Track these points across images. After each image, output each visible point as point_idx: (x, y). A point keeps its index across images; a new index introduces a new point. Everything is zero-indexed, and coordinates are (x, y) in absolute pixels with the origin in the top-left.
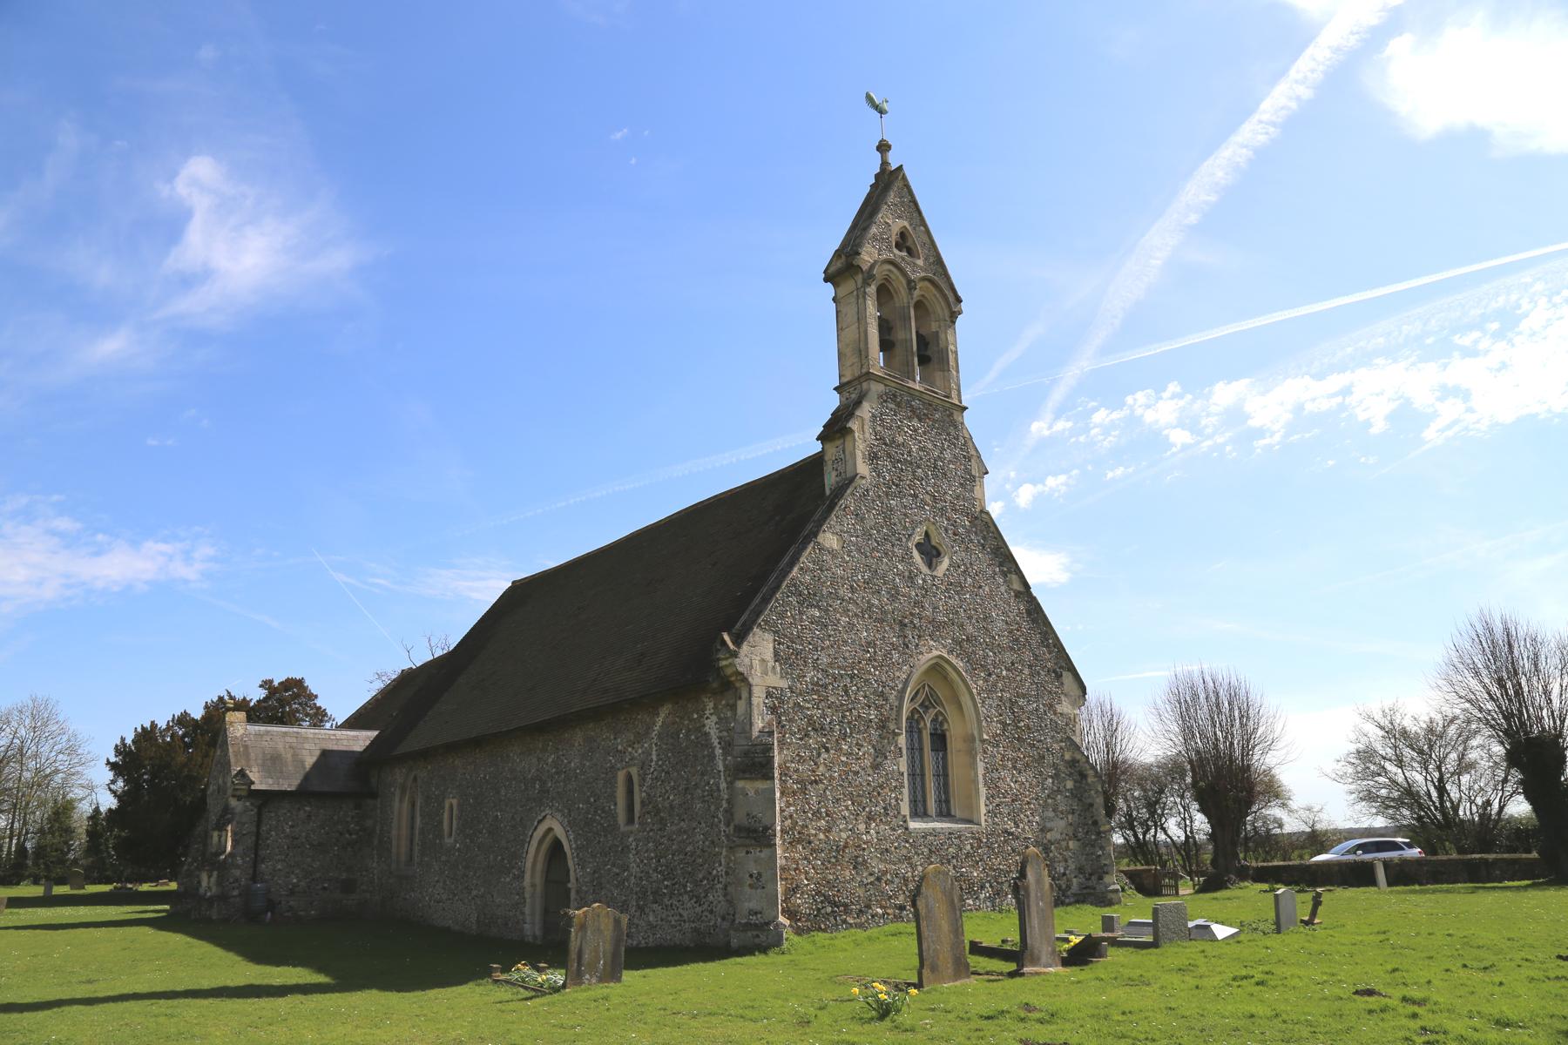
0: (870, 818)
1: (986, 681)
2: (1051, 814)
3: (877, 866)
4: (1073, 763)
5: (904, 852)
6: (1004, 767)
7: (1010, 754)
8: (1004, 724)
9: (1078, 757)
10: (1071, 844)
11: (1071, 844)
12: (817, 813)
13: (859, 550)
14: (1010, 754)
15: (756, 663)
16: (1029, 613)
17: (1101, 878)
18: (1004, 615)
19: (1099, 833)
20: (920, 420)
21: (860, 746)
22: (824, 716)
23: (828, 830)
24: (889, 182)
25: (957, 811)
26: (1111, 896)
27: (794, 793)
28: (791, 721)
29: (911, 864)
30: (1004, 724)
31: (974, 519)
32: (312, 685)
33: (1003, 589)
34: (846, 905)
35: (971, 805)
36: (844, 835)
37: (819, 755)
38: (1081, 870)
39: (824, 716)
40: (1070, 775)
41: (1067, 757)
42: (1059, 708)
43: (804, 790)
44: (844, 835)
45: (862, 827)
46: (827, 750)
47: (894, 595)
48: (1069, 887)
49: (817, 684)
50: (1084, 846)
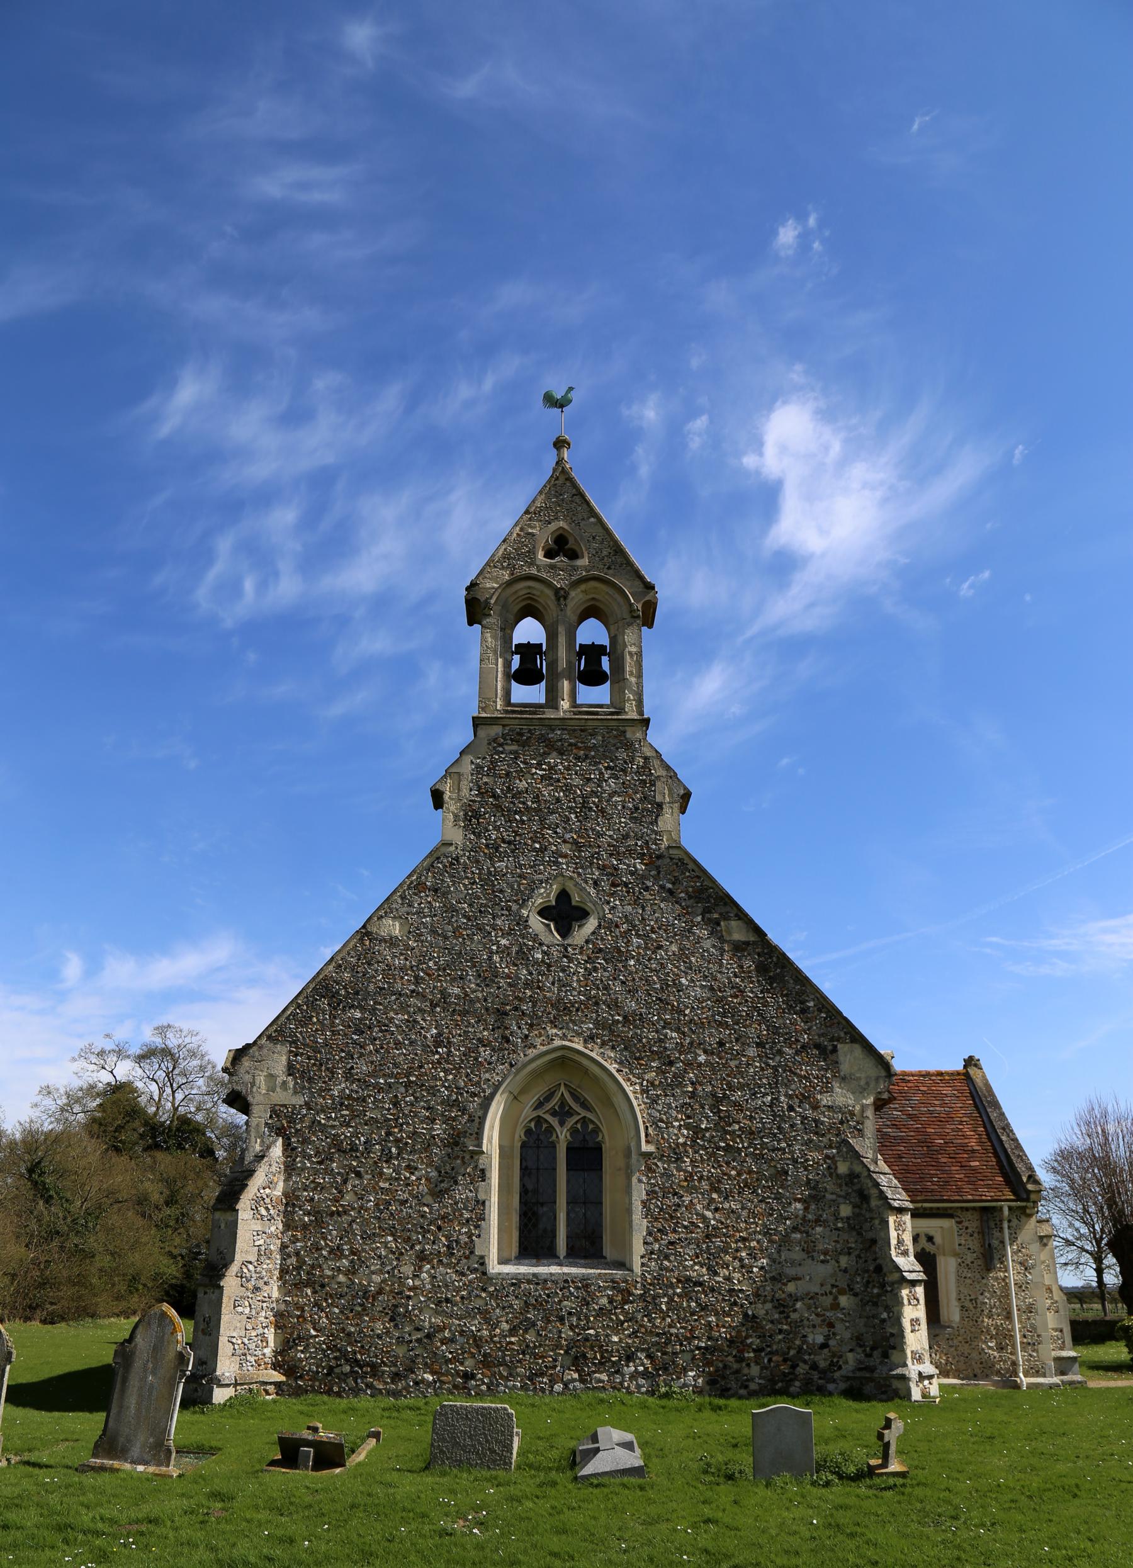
0: (422, 1257)
1: (660, 1072)
2: (797, 1254)
3: (428, 1320)
4: (852, 1177)
5: (478, 1303)
6: (691, 1189)
7: (707, 1170)
8: (697, 1131)
9: (858, 1169)
10: (844, 1300)
11: (844, 1300)
12: (337, 1252)
13: (433, 932)
14: (707, 1170)
15: (261, 1080)
16: (762, 969)
17: (886, 1355)
18: (701, 976)
19: (882, 1286)
20: (561, 753)
21: (411, 1169)
22: (356, 1135)
23: (352, 1272)
24: (564, 491)
25: (608, 1251)
26: (896, 1384)
27: (305, 1227)
28: (305, 1141)
29: (487, 1320)
30: (697, 1131)
31: (654, 860)
32: (982, 1063)
33: (707, 944)
34: (373, 1366)
35: (627, 1246)
36: (377, 1278)
37: (345, 1181)
38: (859, 1340)
39: (356, 1135)
40: (846, 1197)
41: (843, 1168)
42: (825, 1100)
43: (319, 1223)
44: (377, 1278)
45: (408, 1270)
46: (359, 1175)
47: (488, 977)
48: (834, 1366)
49: (349, 1097)
50: (864, 1304)
